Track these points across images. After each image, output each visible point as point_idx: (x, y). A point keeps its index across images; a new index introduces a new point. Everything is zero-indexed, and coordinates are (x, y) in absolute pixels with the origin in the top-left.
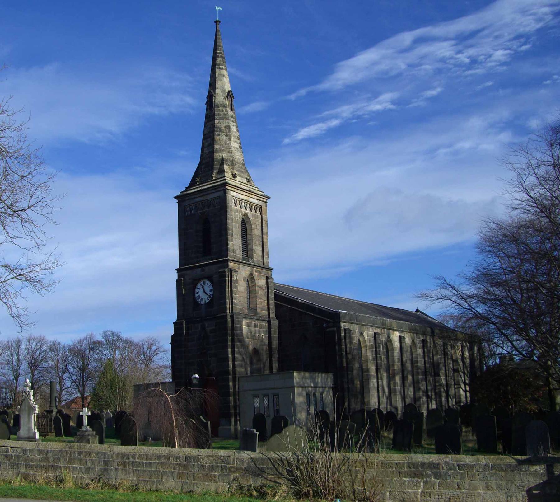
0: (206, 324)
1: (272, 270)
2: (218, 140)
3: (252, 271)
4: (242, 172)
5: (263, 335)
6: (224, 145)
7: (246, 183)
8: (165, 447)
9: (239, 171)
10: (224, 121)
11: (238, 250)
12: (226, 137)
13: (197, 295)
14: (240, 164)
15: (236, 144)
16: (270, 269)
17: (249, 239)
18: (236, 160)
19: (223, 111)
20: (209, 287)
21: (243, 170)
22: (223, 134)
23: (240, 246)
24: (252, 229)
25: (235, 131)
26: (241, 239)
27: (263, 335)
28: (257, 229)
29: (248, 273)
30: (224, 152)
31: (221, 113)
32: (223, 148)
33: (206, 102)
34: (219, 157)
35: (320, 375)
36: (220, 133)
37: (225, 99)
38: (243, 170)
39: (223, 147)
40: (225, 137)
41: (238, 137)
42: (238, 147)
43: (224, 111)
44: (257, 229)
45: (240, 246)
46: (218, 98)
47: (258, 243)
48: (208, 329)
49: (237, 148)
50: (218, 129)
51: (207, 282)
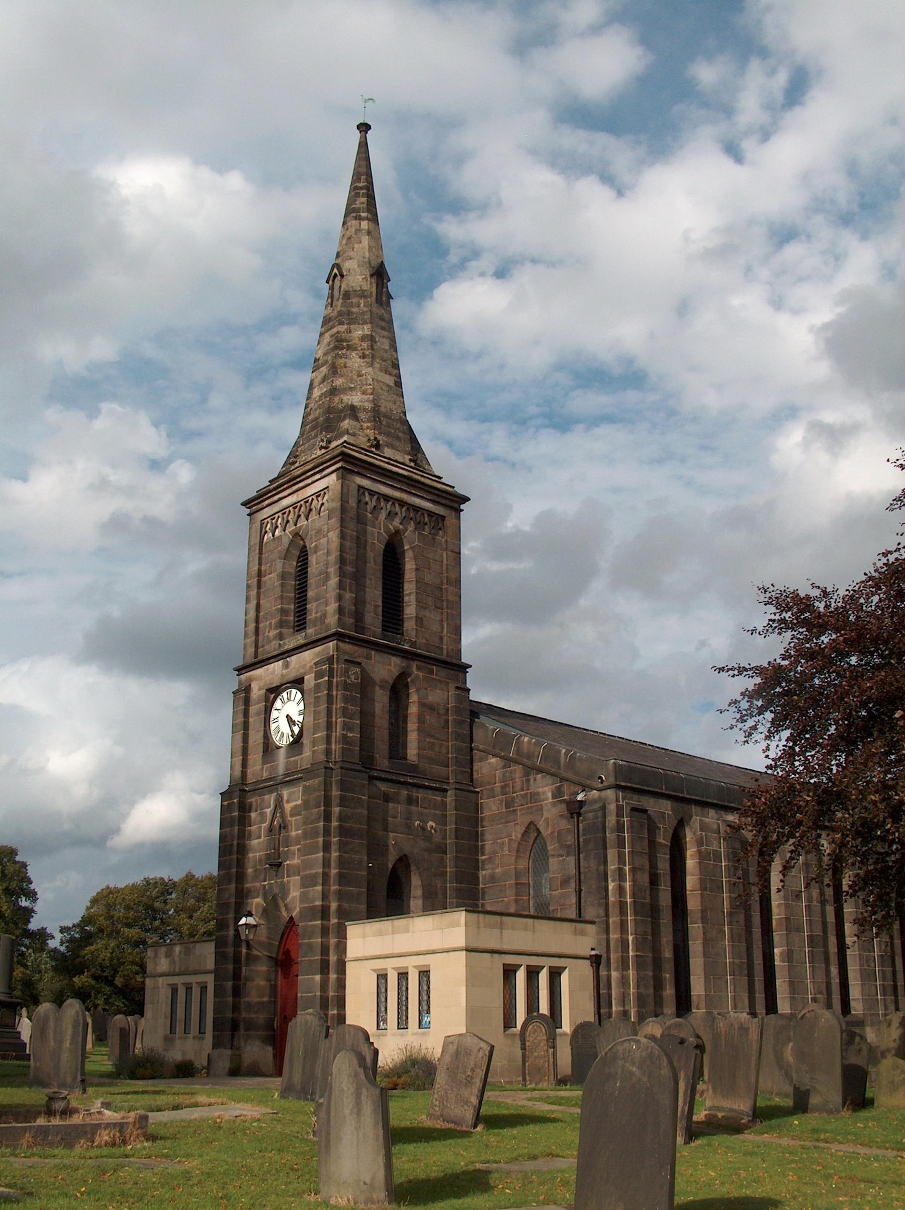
0: (285, 793)
1: (467, 670)
2: (341, 367)
3: (409, 666)
4: (398, 438)
5: (434, 825)
6: (355, 377)
7: (408, 462)
8: (512, 929)
9: (388, 434)
10: (360, 326)
11: (372, 614)
12: (362, 360)
13: (273, 726)
14: (393, 420)
15: (387, 377)
16: (464, 668)
17: (407, 592)
18: (382, 409)
19: (359, 306)
20: (298, 704)
21: (401, 435)
22: (354, 354)
23: (376, 606)
24: (417, 569)
25: (387, 348)
26: (380, 588)
27: (434, 825)
28: (429, 569)
29: (396, 672)
30: (354, 393)
31: (355, 310)
32: (352, 384)
33: (834, 901)
34: (342, 403)
35: (391, 1066)
36: (348, 353)
37: (367, 280)
38: (401, 435)
39: (352, 381)
40: (358, 360)
41: (392, 362)
42: (392, 384)
43: (362, 305)
44: (429, 569)
45: (376, 606)
46: (349, 278)
47: (431, 603)
48: (288, 807)
49: (388, 386)
50: (345, 344)
51: (294, 691)
